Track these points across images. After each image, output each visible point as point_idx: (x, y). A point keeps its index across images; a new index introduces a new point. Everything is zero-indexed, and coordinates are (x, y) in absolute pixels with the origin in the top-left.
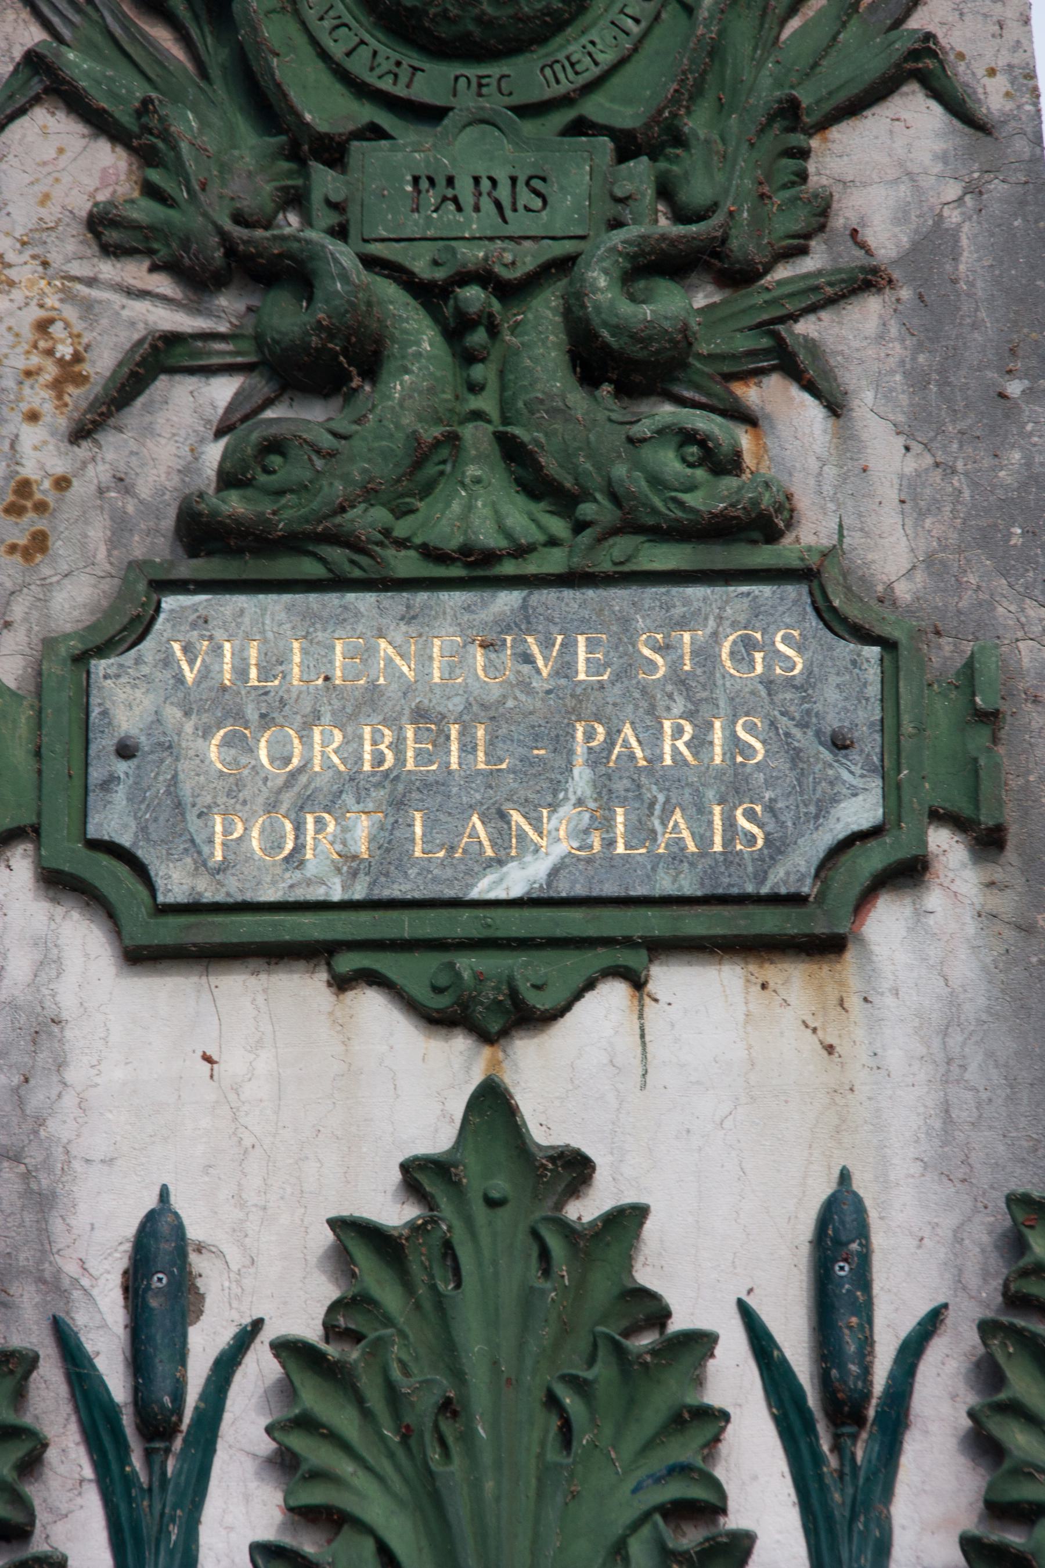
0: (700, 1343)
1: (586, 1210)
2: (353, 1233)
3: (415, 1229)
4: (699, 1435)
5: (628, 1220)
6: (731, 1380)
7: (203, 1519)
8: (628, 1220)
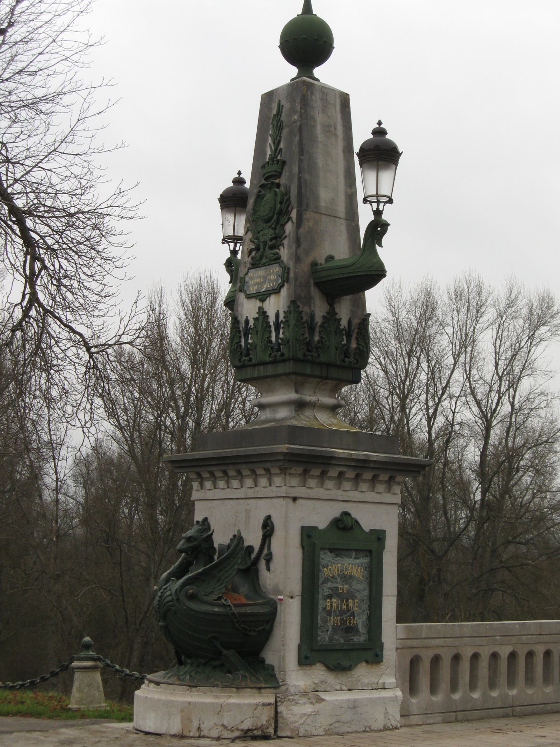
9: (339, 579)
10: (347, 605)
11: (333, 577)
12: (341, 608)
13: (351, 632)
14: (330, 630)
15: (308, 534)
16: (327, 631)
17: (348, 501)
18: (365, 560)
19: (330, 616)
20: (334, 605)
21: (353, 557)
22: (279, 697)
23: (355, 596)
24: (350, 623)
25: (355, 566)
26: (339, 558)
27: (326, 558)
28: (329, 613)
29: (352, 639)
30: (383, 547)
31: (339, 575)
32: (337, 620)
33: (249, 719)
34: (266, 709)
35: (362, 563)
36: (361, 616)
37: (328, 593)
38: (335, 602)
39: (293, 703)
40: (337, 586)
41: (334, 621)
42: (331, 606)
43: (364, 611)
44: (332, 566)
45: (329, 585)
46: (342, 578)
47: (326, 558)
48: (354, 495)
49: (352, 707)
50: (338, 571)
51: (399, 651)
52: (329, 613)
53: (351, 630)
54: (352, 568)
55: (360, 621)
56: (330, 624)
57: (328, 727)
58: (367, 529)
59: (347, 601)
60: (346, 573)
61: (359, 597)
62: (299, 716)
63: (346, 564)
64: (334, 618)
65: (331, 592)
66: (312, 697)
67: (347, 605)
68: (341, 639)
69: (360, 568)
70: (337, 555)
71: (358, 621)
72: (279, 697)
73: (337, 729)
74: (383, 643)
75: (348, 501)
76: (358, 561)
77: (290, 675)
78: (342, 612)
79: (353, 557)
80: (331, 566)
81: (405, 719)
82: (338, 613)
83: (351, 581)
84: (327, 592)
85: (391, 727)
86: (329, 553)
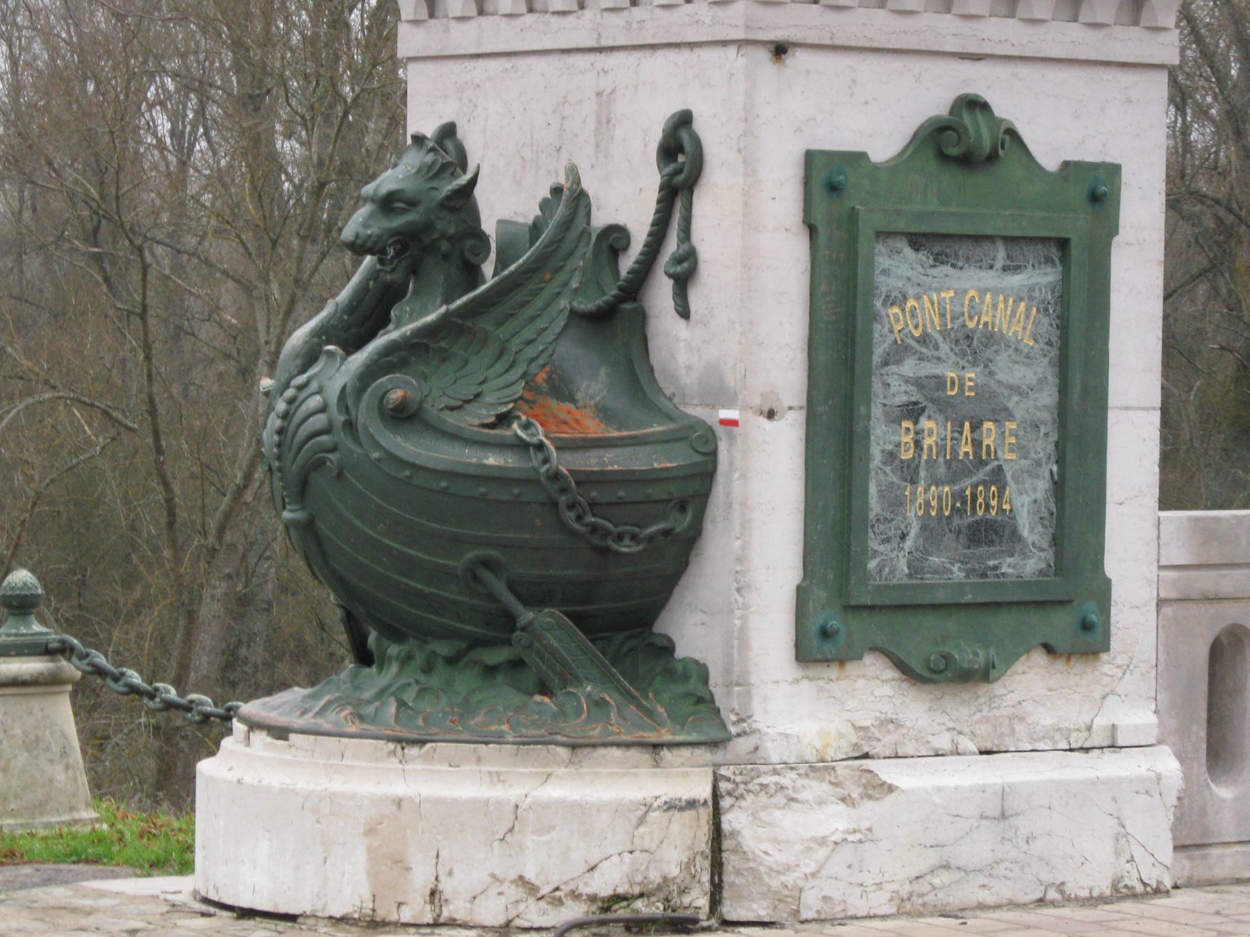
9: (945, 347)
10: (977, 444)
11: (924, 340)
12: (955, 452)
13: (991, 543)
14: (913, 533)
16: (903, 537)
20: (928, 442)
21: (999, 264)
23: (1006, 409)
25: (1003, 299)
27: (896, 267)
28: (909, 472)
29: (995, 568)
31: (944, 333)
32: (940, 499)
33: (615, 859)
35: (1031, 289)
38: (930, 434)
39: (780, 799)
40: (937, 370)
41: (927, 503)
42: (918, 444)
43: (1038, 463)
44: (921, 298)
45: (909, 367)
46: (957, 342)
47: (896, 267)
49: (997, 813)
51: (1168, 610)
52: (909, 472)
55: (1026, 502)
56: (913, 514)
58: (1049, 161)
59: (975, 427)
60: (971, 325)
61: (1019, 414)
63: (972, 293)
64: (926, 490)
67: (977, 444)
68: (955, 569)
69: (1023, 305)
70: (940, 259)
73: (941, 895)
76: (1016, 280)
77: (765, 699)
79: (999, 264)
80: (918, 298)
81: (1191, 858)
82: (942, 470)
83: (989, 353)
84: (901, 394)
85: (1139, 888)
86: (908, 252)
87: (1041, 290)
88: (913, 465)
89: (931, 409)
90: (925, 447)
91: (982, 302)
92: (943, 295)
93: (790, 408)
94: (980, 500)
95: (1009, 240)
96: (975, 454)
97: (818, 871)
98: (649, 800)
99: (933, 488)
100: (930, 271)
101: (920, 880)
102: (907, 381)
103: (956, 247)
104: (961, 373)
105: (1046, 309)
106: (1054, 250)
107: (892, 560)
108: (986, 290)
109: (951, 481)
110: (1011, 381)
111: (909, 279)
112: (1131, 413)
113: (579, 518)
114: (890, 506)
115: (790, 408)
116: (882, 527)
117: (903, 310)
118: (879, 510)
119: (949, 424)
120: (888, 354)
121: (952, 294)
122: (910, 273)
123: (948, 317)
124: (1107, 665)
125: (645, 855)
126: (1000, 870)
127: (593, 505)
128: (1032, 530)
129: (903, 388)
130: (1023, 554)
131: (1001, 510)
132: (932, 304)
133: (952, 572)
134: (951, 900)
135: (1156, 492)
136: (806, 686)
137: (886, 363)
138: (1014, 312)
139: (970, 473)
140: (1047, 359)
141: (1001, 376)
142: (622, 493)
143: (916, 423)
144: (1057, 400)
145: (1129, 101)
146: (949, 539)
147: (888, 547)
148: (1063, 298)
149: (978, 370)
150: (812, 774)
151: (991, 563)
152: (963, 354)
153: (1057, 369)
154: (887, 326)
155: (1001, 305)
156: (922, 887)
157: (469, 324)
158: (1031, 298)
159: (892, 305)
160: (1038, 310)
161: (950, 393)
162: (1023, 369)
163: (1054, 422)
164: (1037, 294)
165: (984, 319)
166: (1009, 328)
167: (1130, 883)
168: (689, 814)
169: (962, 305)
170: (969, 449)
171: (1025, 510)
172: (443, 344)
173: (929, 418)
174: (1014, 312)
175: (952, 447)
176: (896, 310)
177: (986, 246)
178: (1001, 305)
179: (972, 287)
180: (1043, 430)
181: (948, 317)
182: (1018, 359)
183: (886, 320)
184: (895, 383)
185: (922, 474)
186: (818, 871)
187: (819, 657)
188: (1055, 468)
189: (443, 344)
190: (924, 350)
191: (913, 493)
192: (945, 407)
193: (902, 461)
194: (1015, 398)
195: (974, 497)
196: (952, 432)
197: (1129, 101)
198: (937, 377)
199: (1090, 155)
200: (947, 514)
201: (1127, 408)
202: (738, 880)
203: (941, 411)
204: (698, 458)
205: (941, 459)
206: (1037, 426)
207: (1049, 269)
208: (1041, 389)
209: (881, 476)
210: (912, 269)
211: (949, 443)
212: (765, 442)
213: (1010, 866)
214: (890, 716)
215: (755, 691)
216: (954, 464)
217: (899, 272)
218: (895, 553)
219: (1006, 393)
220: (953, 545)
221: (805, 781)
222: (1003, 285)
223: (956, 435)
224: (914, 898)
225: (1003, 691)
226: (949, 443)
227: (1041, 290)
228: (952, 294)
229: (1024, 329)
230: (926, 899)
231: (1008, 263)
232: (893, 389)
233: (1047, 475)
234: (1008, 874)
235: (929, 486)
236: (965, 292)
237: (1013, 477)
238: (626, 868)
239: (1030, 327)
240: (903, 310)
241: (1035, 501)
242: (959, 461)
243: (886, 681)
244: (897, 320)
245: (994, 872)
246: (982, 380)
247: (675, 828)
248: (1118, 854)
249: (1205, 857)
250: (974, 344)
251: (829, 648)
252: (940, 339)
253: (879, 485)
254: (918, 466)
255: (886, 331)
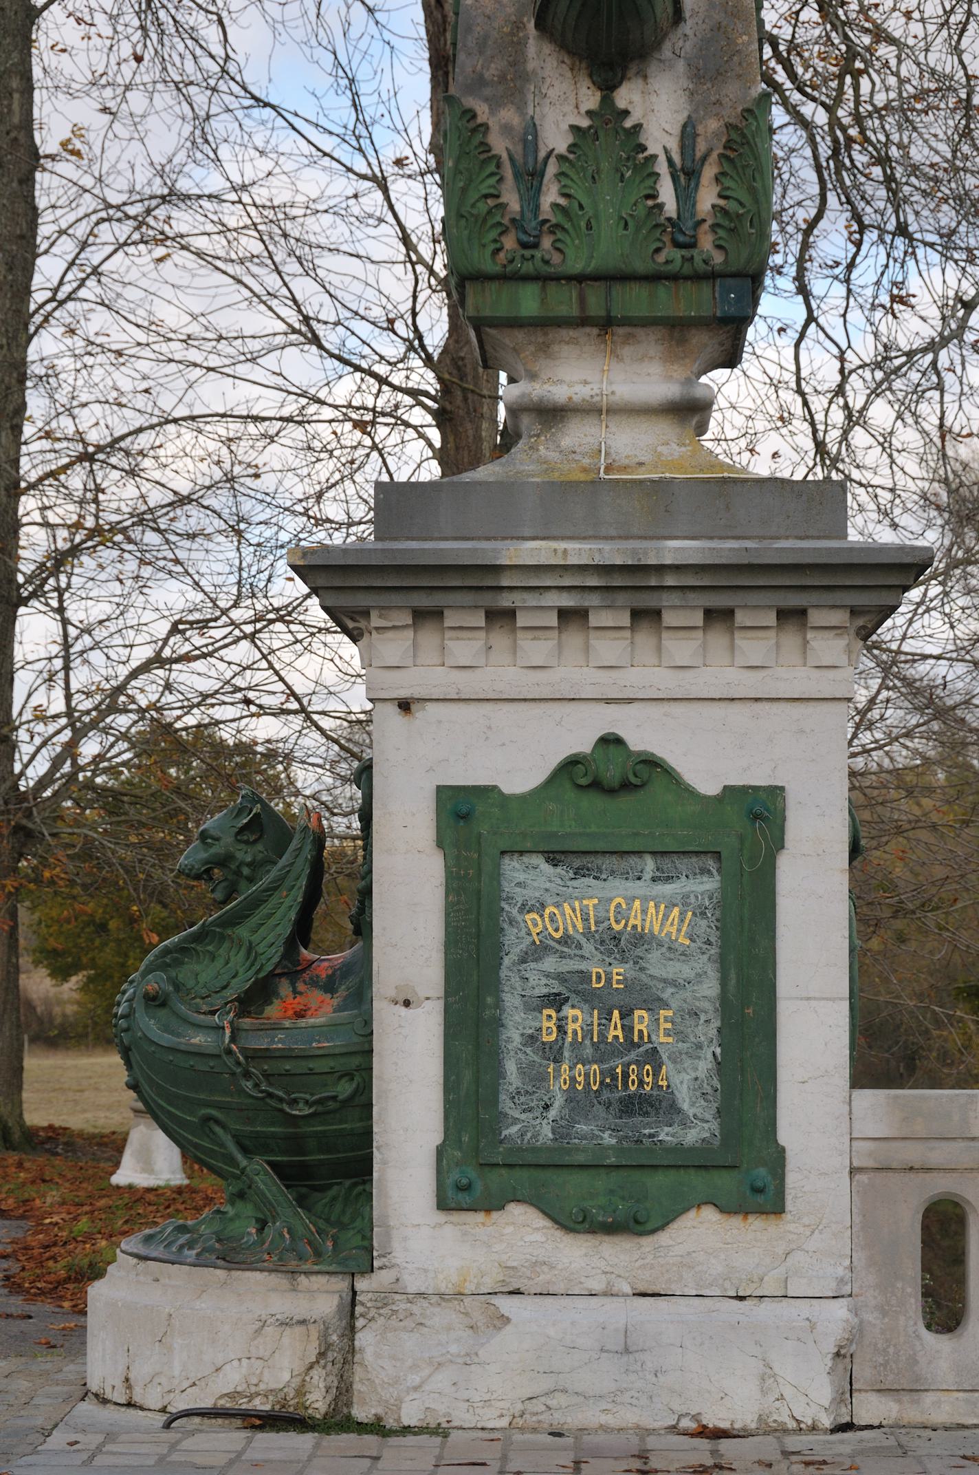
0: (654, 157)
1: (628, 124)
2: (574, 129)
3: (590, 127)
4: (653, 179)
5: (638, 127)
6: (662, 167)
7: (440, 893)
8: (638, 127)
9: (588, 948)
10: (628, 1030)
11: (566, 940)
12: (602, 1035)
13: (647, 1114)
14: (557, 1104)
15: (464, 815)
16: (547, 1107)
17: (630, 701)
18: (706, 886)
19: (557, 1060)
20: (571, 1027)
21: (647, 876)
22: (363, 1304)
23: (660, 999)
24: (641, 1083)
25: (663, 909)
26: (590, 881)
27: (526, 877)
28: (554, 1053)
29: (651, 1136)
30: (778, 844)
31: (588, 934)
32: (587, 1075)
33: (235, 1363)
34: (291, 1337)
35: (686, 896)
36: (688, 1063)
37: (545, 991)
38: (575, 1019)
39: (408, 1323)
40: (583, 966)
41: (573, 1079)
42: (561, 1030)
43: (699, 1046)
44: (551, 905)
45: (550, 964)
46: (602, 942)
47: (526, 877)
48: (647, 676)
49: (620, 1348)
50: (586, 920)
51: (862, 1178)
52: (554, 1053)
53: (657, 1105)
54: (644, 911)
55: (689, 1079)
56: (558, 1088)
57: (519, 1406)
58: (709, 787)
59: (626, 1014)
60: (617, 927)
61: (674, 1004)
62: (409, 1362)
63: (619, 900)
64: (571, 1069)
65: (556, 988)
66: (476, 1307)
67: (628, 1030)
68: (606, 1135)
69: (676, 911)
70: (579, 873)
71: (676, 1080)
72: (363, 1304)
73: (556, 1415)
74: (783, 1150)
75: (630, 701)
76: (668, 889)
77: (405, 1239)
78: (604, 1050)
79: (647, 876)
80: (557, 905)
81: (899, 1401)
82: (588, 1051)
83: (639, 952)
84: (540, 986)
85: (792, 1425)
86: (545, 867)
87: (697, 897)
88: (556, 1047)
89: (574, 999)
90: (570, 1032)
91: (630, 909)
92: (585, 902)
93: (428, 999)
94: (633, 1077)
95: (653, 853)
96: (625, 1037)
97: (420, 1386)
98: (264, 1317)
99: (580, 1066)
100: (569, 883)
101: (534, 1401)
102: (548, 976)
103: (600, 862)
104: (608, 969)
105: (703, 914)
106: (711, 862)
107: (534, 1127)
108: (634, 898)
109: (599, 1061)
110: (665, 975)
111: (547, 890)
112: (814, 1003)
113: (256, 1085)
114: (531, 1080)
115: (428, 999)
116: (523, 1099)
117: (542, 916)
118: (520, 1084)
119: (596, 1012)
120: (526, 953)
121: (596, 901)
122: (548, 885)
123: (592, 921)
124: (790, 1225)
125: (260, 1362)
126: (626, 1398)
127: (267, 1076)
128: (693, 1104)
129: (544, 981)
130: (684, 1124)
131: (656, 1085)
132: (574, 910)
133: (602, 1139)
134: (569, 1420)
135: (846, 1073)
136: (449, 1231)
137: (523, 961)
138: (666, 917)
139: (621, 1054)
140: (705, 957)
141: (652, 971)
142: (288, 1067)
143: (558, 1011)
144: (719, 991)
145: (802, 731)
146: (599, 1110)
147: (530, 1115)
148: (724, 903)
149: (627, 966)
150: (444, 1304)
151: (647, 1131)
152: (610, 953)
153: (718, 965)
154: (524, 930)
155: (652, 910)
156: (530, 1406)
157: (229, 932)
158: (685, 904)
159: (529, 912)
160: (694, 914)
161: (595, 985)
162: (678, 964)
163: (716, 1010)
164: (692, 900)
165: (632, 922)
166: (661, 930)
167: (780, 1419)
168: (299, 1330)
169: (608, 911)
170: (619, 1033)
171: (685, 1086)
172: (210, 948)
173: (573, 1007)
174: (666, 917)
175: (600, 1033)
176: (534, 916)
177: (633, 860)
178: (652, 910)
179: (618, 896)
180: (703, 1017)
181: (592, 921)
182: (672, 956)
183: (523, 925)
184: (534, 978)
185: (566, 1054)
186: (420, 1386)
187: (453, 1205)
188: (718, 1051)
189: (210, 948)
190: (566, 950)
191: (557, 1071)
192: (590, 998)
193: (543, 1043)
194: (670, 990)
195: (626, 1075)
196: (599, 1019)
197: (802, 731)
198: (582, 972)
199: (759, 779)
200: (595, 1088)
201: (808, 999)
202: (363, 1389)
203: (586, 1001)
204: (356, 1039)
205: (587, 1042)
206: (696, 1014)
207: (705, 879)
208: (701, 982)
209: (520, 1055)
210: (550, 881)
211: (596, 1028)
212: (400, 1026)
213: (636, 1395)
214: (541, 1259)
215: (394, 1233)
216: (602, 1046)
217: (536, 884)
218: (538, 1121)
219: (661, 985)
220: (604, 1115)
221: (437, 1310)
222: (654, 893)
223: (603, 1021)
224: (527, 1416)
225: (671, 1243)
226: (596, 1028)
227: (697, 897)
228: (596, 901)
229: (679, 930)
230: (541, 1417)
231: (658, 874)
232: (532, 982)
233: (710, 1056)
234: (634, 1401)
235: (575, 1065)
236: (611, 900)
237: (669, 1058)
238: (244, 1371)
239: (684, 929)
240: (542, 916)
241: (696, 1079)
242: (607, 1043)
243: (537, 1229)
244: (536, 925)
245: (618, 1399)
246: (631, 974)
247: (286, 1340)
248: (764, 1392)
249: (917, 1402)
250: (619, 944)
251: (464, 1198)
252: (583, 941)
253: (519, 1063)
254: (561, 1048)
255: (523, 933)
